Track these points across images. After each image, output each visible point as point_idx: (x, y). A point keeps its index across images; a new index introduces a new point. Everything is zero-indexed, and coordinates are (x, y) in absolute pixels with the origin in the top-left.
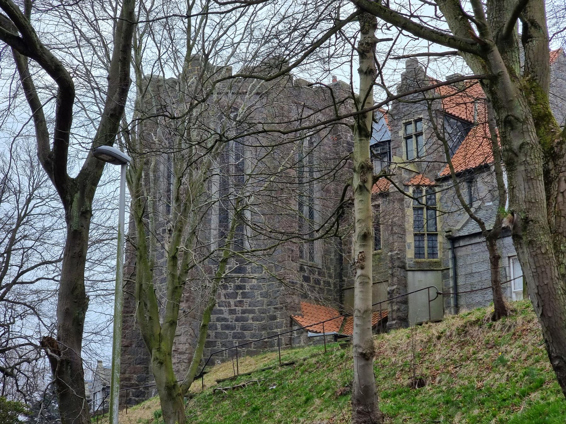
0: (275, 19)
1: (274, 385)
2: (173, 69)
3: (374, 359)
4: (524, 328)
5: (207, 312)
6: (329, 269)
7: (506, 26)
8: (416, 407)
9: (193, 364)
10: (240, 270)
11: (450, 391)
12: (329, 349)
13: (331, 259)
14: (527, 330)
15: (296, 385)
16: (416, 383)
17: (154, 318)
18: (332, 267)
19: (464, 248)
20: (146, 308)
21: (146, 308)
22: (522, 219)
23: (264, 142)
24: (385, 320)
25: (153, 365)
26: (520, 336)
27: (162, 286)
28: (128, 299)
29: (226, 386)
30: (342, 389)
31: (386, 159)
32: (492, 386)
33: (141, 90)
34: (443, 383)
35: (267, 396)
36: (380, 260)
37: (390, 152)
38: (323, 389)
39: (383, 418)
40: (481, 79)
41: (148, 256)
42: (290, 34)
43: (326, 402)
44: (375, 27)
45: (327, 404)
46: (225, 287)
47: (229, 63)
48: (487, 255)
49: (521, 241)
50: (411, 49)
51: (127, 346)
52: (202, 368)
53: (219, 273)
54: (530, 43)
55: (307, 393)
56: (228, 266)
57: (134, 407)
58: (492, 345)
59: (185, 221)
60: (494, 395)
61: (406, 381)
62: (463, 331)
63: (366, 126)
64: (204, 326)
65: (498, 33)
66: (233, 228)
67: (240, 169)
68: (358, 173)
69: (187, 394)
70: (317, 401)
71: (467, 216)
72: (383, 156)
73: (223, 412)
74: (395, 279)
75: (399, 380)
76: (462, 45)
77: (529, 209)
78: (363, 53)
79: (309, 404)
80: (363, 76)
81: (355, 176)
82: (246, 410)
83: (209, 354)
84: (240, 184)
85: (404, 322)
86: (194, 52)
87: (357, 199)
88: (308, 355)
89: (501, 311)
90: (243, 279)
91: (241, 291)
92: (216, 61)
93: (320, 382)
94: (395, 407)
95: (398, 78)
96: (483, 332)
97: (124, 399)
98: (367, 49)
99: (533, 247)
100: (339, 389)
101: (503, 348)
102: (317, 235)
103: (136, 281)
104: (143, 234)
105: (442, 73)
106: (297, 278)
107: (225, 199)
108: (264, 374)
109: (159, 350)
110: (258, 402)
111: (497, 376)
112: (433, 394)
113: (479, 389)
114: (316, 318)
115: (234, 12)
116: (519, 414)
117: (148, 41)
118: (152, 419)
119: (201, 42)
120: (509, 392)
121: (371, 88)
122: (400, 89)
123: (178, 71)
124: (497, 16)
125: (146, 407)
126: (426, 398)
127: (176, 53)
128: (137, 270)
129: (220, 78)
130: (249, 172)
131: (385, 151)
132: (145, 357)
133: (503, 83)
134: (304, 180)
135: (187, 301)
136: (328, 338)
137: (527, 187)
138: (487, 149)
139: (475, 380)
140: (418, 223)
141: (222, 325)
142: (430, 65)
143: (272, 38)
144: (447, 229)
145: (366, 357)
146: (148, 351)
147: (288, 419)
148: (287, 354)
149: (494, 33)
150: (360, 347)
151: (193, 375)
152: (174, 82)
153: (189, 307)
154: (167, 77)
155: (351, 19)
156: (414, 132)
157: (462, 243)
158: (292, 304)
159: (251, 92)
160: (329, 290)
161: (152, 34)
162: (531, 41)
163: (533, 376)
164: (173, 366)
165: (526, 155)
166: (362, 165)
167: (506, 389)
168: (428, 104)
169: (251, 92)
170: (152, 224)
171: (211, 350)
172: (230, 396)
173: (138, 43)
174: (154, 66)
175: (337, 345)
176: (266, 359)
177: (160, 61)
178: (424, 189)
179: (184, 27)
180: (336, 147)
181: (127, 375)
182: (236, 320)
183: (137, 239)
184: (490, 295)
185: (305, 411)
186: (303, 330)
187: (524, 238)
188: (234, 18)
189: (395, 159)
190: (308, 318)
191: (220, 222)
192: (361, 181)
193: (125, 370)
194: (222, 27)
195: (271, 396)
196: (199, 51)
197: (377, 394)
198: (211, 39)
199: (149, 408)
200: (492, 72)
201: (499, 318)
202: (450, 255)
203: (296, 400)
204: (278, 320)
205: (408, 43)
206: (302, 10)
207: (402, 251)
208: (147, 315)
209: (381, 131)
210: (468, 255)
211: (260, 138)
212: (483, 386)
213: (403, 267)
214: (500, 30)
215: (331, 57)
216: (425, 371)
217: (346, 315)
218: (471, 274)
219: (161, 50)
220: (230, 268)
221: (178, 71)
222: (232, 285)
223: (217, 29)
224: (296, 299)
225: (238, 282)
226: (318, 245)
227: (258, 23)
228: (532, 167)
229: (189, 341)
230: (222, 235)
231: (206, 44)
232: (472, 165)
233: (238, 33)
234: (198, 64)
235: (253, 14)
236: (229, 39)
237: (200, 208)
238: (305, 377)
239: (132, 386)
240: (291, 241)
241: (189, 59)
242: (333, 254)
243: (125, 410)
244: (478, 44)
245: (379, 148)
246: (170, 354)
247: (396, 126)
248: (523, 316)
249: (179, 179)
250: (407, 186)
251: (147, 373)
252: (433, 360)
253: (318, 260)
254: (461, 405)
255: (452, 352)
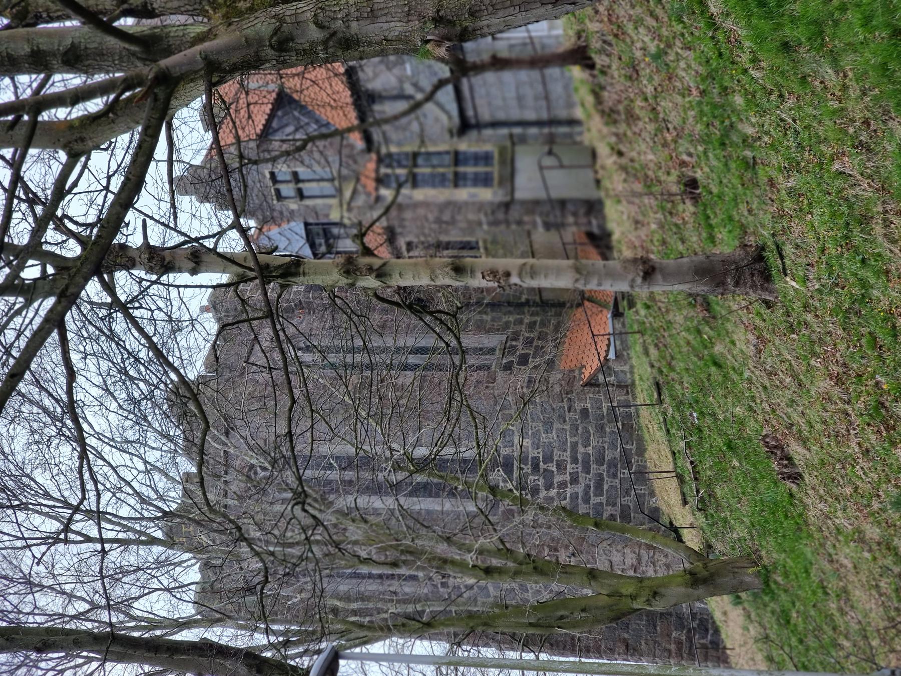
0: (107, 404)
1: (691, 415)
2: (186, 568)
3: (652, 256)
4: (606, 19)
5: (575, 521)
6: (507, 325)
7: (127, 46)
8: (729, 194)
9: (657, 543)
10: (507, 466)
11: (705, 140)
12: (636, 327)
13: (493, 320)
14: (609, 15)
15: (692, 380)
16: (691, 193)
17: (583, 604)
18: (505, 319)
19: (480, 110)
20: (567, 617)
21: (567, 617)
22: (435, 27)
23: (306, 423)
24: (591, 236)
25: (658, 606)
26: (619, 26)
27: (532, 589)
28: (552, 645)
29: (692, 491)
30: (699, 308)
31: (335, 231)
32: (697, 73)
33: (218, 621)
34: (692, 150)
35: (709, 427)
36: (495, 242)
37: (323, 224)
38: (698, 339)
39: (746, 245)
40: (211, 87)
41: (483, 612)
42: (132, 379)
43: (719, 335)
44: (123, 247)
45: (723, 332)
46: (535, 491)
47: (178, 478)
48: (490, 76)
49: (470, 29)
50: (160, 189)
51: (627, 646)
52: (663, 528)
53: (512, 500)
54: (155, 6)
55: (706, 364)
56: (501, 484)
57: (723, 636)
58: (633, 72)
59: (431, 553)
60: (713, 70)
61: (688, 208)
62: (610, 115)
63: (282, 265)
64: (596, 525)
65: (138, 58)
66: (441, 477)
67: (347, 463)
68: (356, 280)
69: (705, 554)
70: (718, 348)
71: (429, 107)
72: (329, 235)
73: (733, 497)
74: (526, 219)
75: (686, 219)
76: (158, 118)
77: (419, 15)
78: (165, 266)
79: (722, 361)
80: (204, 268)
81: (361, 283)
82: (731, 461)
83: (642, 516)
84: (368, 462)
85: (593, 207)
86: (159, 534)
87: (397, 281)
88: (644, 359)
89: (579, 55)
90: (523, 460)
91: (541, 463)
92: (175, 497)
93: (688, 343)
94: (729, 227)
95: (206, 209)
96: (612, 84)
97: (712, 652)
98: (160, 261)
99: (480, 10)
100: (699, 313)
101: (638, 54)
102: (454, 343)
103: (524, 632)
104: (449, 620)
105: (199, 140)
106: (522, 375)
107: (396, 488)
108: (674, 431)
109: (633, 597)
110: (719, 442)
111: (682, 64)
112: (709, 167)
113: (703, 93)
114: (586, 347)
115: (95, 469)
116: (743, 33)
117: (141, 607)
118: (744, 609)
119: (144, 523)
120: (707, 48)
121: (221, 256)
122: (222, 207)
123: (189, 560)
124: (110, 59)
125: (723, 618)
126: (715, 177)
127: (159, 563)
128: (506, 630)
129: (200, 493)
130: (352, 450)
131: (321, 232)
132: (645, 618)
133: (219, 52)
134: (366, 361)
135: (556, 550)
136: (618, 326)
137: (384, 19)
138: (320, 73)
139: (687, 99)
140: (438, 181)
141: (595, 495)
142: (186, 159)
143: (140, 410)
144: (447, 136)
145: (649, 272)
146: (634, 614)
147: (747, 395)
148: (643, 394)
149: (139, 64)
150: (633, 280)
151: (675, 544)
152: (206, 566)
153: (567, 547)
154: (197, 577)
155: (109, 288)
156: (292, 186)
157: (470, 113)
158: (563, 382)
159: (225, 444)
160: (543, 324)
161: (128, 602)
162: (152, 4)
163: (682, 9)
164: (660, 575)
165: (334, 19)
166: (344, 272)
167: (703, 52)
168: (247, 164)
169: (225, 444)
170: (434, 605)
171: (635, 512)
172: (709, 486)
173: (143, 623)
174: (180, 599)
175: (629, 314)
176: (650, 426)
177: (173, 588)
178: (383, 170)
179: (118, 550)
180: (314, 312)
181: (673, 647)
182: (588, 472)
183: (457, 630)
184: (554, 72)
185: (734, 369)
186: (605, 367)
187: (465, 24)
188: (106, 469)
189: (335, 216)
190: (586, 359)
191: (430, 496)
192: (370, 274)
193: (665, 650)
194: (120, 489)
195: (708, 420)
196: (157, 525)
197: (708, 253)
198: (138, 506)
199: (725, 613)
200: (200, 70)
201: (590, 58)
202: (488, 132)
203: (716, 381)
204: (589, 406)
205: (152, 198)
206: (94, 360)
207: (480, 207)
208: (579, 616)
209: (289, 240)
210: (490, 104)
211: (298, 431)
212: (698, 88)
213: (507, 206)
214: (134, 54)
215: (170, 317)
216: (673, 178)
217: (583, 299)
218: (520, 99)
219: (155, 586)
220: (505, 481)
221: (189, 560)
222: (531, 478)
223: (122, 496)
224: (555, 377)
225: (527, 469)
226: (469, 340)
227: (114, 430)
228: (353, 9)
229: (619, 547)
230: (452, 493)
231: (146, 514)
232: (346, 96)
233: (129, 463)
234: (177, 527)
235: (100, 439)
236: (139, 478)
237: (408, 527)
238: (680, 365)
239: (690, 640)
240: (463, 385)
241: (170, 542)
242: (485, 317)
243: (728, 652)
244: (156, 91)
245: (317, 241)
246: (641, 580)
247: (281, 213)
248: (587, 21)
249: (361, 562)
250: (378, 199)
251: (670, 614)
252: (656, 164)
253: (493, 340)
254: (727, 123)
255: (644, 134)
